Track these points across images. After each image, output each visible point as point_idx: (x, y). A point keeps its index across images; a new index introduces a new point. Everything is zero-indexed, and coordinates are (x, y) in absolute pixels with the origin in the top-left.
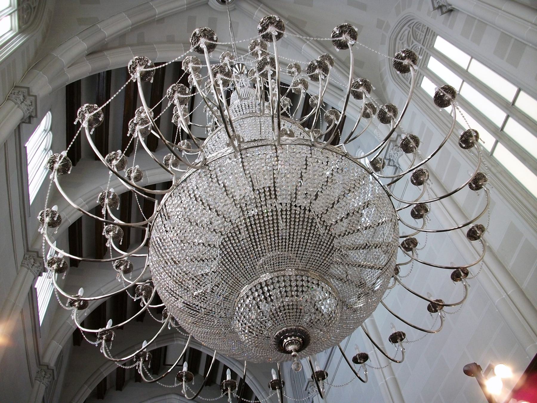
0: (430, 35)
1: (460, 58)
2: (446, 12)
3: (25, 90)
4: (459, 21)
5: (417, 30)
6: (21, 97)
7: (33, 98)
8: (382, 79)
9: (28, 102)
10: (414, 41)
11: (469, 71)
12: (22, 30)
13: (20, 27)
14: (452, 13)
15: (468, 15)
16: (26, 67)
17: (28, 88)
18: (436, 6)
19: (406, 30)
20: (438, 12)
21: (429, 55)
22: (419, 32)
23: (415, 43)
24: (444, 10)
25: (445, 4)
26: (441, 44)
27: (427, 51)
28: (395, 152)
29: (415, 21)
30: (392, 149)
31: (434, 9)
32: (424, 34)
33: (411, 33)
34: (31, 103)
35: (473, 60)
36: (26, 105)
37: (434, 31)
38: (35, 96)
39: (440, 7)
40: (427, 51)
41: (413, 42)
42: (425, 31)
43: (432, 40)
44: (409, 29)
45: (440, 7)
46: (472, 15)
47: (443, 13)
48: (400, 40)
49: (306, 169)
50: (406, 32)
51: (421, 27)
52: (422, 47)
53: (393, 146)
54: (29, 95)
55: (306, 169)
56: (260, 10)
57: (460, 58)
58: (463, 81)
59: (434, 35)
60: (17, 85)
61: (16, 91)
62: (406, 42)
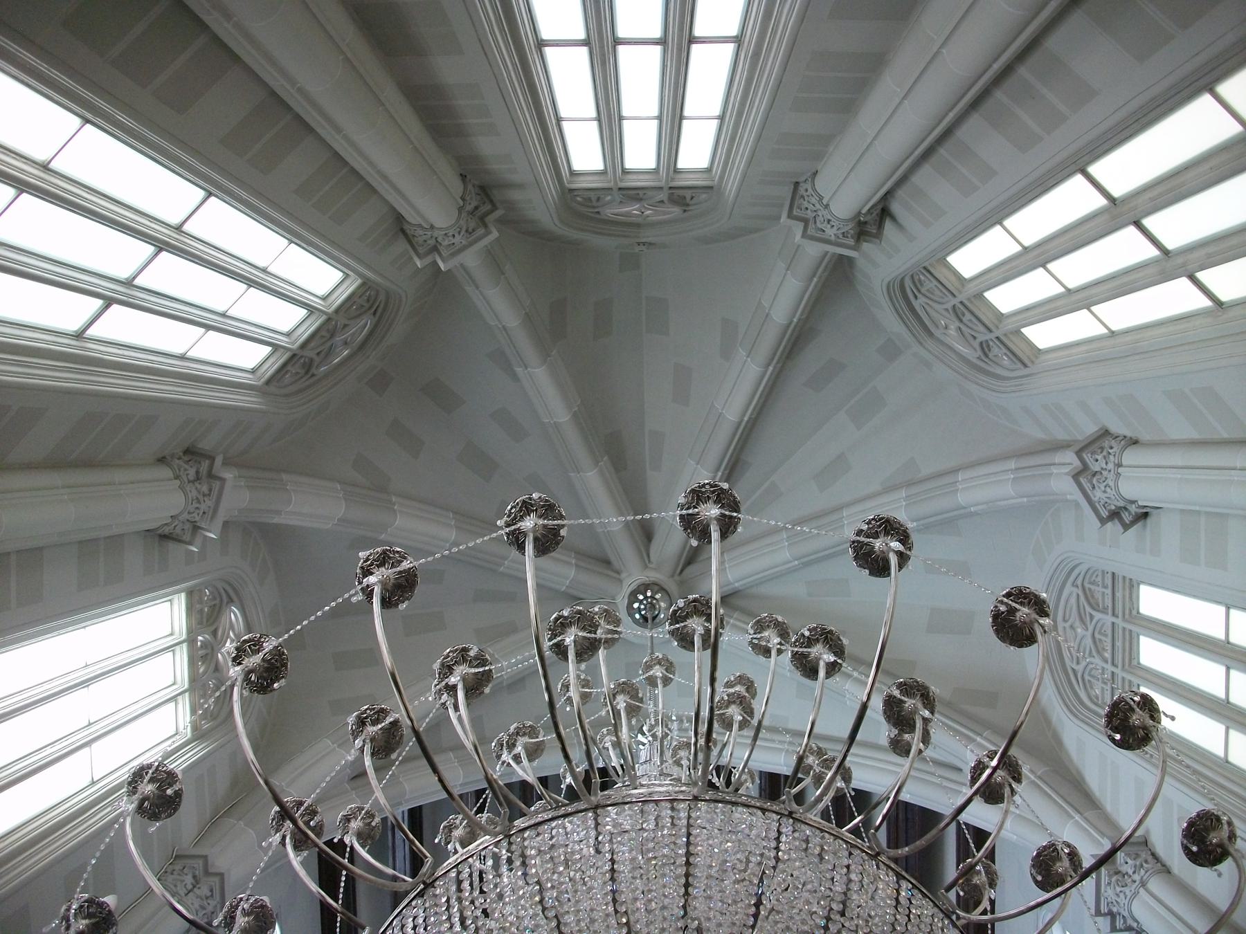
0: (1123, 589)
1: (1202, 616)
2: (1134, 522)
3: (199, 864)
4: (1167, 529)
5: (1092, 587)
6: (189, 880)
7: (217, 879)
8: (1048, 721)
9: (204, 891)
10: (1094, 613)
11: (1232, 640)
12: (199, 735)
13: (195, 728)
14: (1149, 520)
15: (1182, 511)
16: (208, 816)
17: (205, 857)
18: (1105, 514)
19: (1070, 594)
20: (1113, 527)
21: (1134, 635)
22: (1098, 590)
23: (1097, 616)
24: (1127, 518)
25: (1121, 504)
26: (1153, 602)
27: (1128, 626)
28: (1118, 889)
29: (1083, 568)
30: (1109, 884)
31: (1103, 521)
32: (1109, 591)
33: (1082, 598)
34: (211, 891)
35: (1233, 612)
36: (197, 897)
37: (1128, 576)
38: (221, 875)
39: (1115, 515)
40: (1128, 626)
41: (1092, 617)
42: (1110, 583)
43: (1131, 598)
44: (1075, 589)
45: (1115, 515)
46: (1181, 507)
47: (1126, 527)
48: (1065, 620)
49: (774, 868)
50: (1073, 601)
51: (1099, 579)
52: (1114, 620)
53: (1110, 876)
54: (207, 873)
55: (774, 868)
56: (734, 626)
57: (1202, 616)
58: (1228, 669)
59: (1132, 586)
60: (180, 853)
61: (178, 867)
62: (1078, 623)
